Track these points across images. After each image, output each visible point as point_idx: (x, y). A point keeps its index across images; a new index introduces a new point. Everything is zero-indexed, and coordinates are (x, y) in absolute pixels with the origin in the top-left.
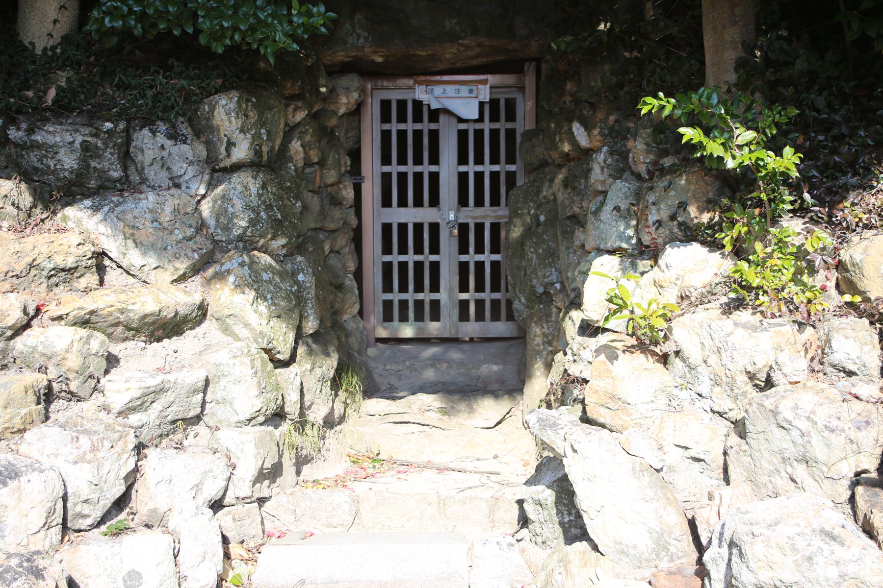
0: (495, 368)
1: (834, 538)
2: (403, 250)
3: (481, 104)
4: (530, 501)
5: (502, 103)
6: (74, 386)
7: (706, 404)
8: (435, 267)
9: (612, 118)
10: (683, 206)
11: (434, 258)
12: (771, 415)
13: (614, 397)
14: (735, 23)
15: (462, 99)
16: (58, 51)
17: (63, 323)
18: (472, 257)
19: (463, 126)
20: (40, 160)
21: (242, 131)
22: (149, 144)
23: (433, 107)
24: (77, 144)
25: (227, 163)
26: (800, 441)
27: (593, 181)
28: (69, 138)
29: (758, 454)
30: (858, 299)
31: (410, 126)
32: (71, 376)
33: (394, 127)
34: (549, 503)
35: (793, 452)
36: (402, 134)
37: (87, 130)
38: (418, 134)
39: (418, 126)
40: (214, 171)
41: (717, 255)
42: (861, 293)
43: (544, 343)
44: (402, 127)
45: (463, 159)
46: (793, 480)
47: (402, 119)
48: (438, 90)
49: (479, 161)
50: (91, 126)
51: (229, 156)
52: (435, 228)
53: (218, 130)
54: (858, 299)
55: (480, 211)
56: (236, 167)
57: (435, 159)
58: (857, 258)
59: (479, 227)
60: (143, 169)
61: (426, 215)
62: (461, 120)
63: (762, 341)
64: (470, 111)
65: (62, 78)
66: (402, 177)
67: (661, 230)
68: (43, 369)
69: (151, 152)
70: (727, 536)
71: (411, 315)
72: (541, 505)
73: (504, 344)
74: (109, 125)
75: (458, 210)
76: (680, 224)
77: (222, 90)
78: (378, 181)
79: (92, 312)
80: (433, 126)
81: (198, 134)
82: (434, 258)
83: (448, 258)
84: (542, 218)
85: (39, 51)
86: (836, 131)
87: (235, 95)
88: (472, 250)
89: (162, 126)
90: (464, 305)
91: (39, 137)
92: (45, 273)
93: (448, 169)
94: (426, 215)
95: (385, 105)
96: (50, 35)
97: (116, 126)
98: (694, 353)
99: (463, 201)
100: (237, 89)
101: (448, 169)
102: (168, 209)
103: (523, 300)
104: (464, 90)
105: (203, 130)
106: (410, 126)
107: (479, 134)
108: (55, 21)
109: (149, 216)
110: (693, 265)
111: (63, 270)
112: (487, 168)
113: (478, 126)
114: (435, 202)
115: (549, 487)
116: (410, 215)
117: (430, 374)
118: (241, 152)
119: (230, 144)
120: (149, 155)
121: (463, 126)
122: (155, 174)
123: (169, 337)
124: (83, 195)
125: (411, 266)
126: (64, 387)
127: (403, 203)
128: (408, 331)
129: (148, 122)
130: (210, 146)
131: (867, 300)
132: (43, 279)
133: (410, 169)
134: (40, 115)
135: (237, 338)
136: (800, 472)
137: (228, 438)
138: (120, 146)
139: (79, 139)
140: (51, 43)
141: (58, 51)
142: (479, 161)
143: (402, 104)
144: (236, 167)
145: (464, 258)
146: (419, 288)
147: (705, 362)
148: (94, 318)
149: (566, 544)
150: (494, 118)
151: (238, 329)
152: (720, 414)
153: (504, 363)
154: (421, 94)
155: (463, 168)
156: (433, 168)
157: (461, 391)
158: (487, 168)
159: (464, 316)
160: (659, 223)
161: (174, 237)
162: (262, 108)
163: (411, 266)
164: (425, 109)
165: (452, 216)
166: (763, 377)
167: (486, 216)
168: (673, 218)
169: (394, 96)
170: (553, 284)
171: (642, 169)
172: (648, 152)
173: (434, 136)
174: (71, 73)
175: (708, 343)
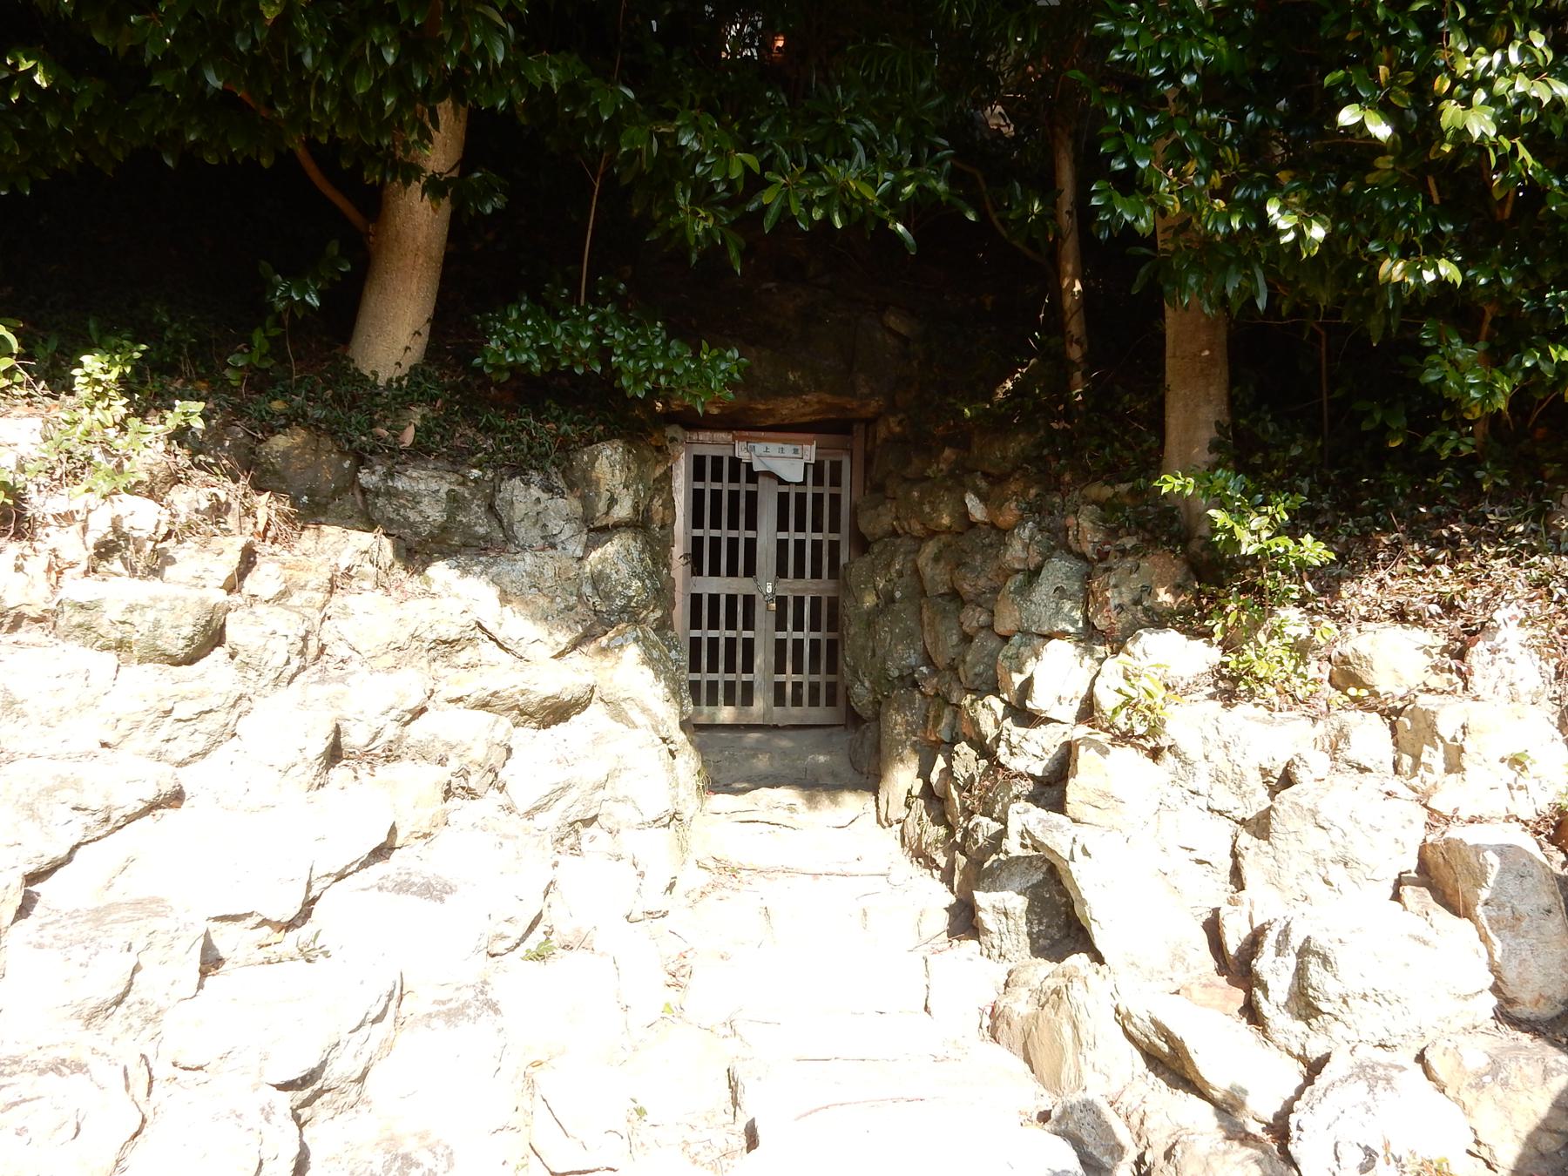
0: (822, 759)
1: (1425, 943)
2: (714, 624)
3: (806, 465)
4: (990, 909)
5: (827, 466)
6: (473, 782)
7: (1202, 802)
8: (749, 645)
9: (1033, 492)
10: (1148, 590)
11: (748, 634)
12: (1309, 814)
13: (1105, 795)
14: (1210, 402)
15: (786, 460)
16: (404, 383)
17: (461, 704)
18: (790, 635)
19: (784, 489)
20: (397, 511)
21: (626, 487)
22: (522, 496)
23: (756, 469)
24: (442, 494)
25: (610, 521)
26: (1339, 841)
27: (1008, 557)
28: (434, 486)
29: (1285, 856)
30: (1364, 693)
31: (725, 486)
32: (473, 769)
33: (708, 486)
34: (1018, 912)
35: (1329, 853)
36: (716, 494)
37: (453, 477)
38: (734, 496)
39: (734, 487)
40: (590, 530)
41: (1200, 643)
42: (1365, 686)
43: (906, 733)
44: (717, 486)
45: (782, 525)
46: (1327, 882)
47: (717, 477)
48: (760, 448)
49: (800, 527)
50: (456, 472)
51: (607, 513)
52: (749, 600)
53: (598, 484)
54: (1364, 693)
55: (799, 584)
56: (617, 527)
57: (752, 524)
58: (1363, 651)
59: (799, 602)
60: (511, 525)
61: (739, 586)
62: (781, 482)
63: (1261, 735)
64: (792, 471)
65: (416, 415)
66: (715, 542)
67: (1123, 615)
68: (442, 761)
69: (522, 506)
70: (1296, 941)
71: (721, 698)
72: (1006, 914)
73: (822, 732)
74: (476, 473)
75: (776, 582)
76: (1146, 610)
77: (607, 437)
78: (773, 549)
79: (494, 694)
80: (751, 487)
81: (572, 486)
82: (748, 634)
83: (763, 636)
84: (898, 594)
85: (381, 382)
86: (1321, 521)
87: (618, 443)
88: (790, 626)
89: (536, 477)
90: (779, 688)
91: (401, 484)
92: (426, 645)
93: (767, 535)
94: (739, 586)
95: (699, 462)
96: (398, 364)
97: (485, 474)
98: (1193, 750)
99: (781, 572)
100: (620, 437)
101: (767, 535)
102: (549, 572)
103: (867, 684)
104: (789, 449)
105: (579, 483)
106: (725, 486)
107: (801, 498)
108: (407, 348)
109: (526, 580)
110: (1172, 655)
111: (444, 642)
112: (809, 536)
113: (801, 490)
114: (750, 571)
115: (1019, 893)
116: (721, 586)
117: (762, 763)
118: (623, 511)
119: (613, 501)
120: (520, 509)
121: (784, 489)
122: (524, 532)
123: (556, 723)
124: (441, 553)
125: (722, 642)
126: (463, 783)
127: (715, 571)
128: (726, 714)
129: (518, 470)
130: (587, 503)
131: (1376, 694)
132: (424, 653)
133: (724, 533)
134: (399, 458)
135: (633, 725)
136: (1337, 873)
137: (631, 842)
138: (486, 496)
139: (445, 487)
140: (399, 373)
141: (404, 383)
142: (800, 527)
143: (717, 461)
144: (617, 527)
145: (781, 635)
146: (730, 668)
147: (1206, 757)
148: (494, 701)
149: (1037, 951)
150: (818, 481)
151: (635, 714)
152: (1220, 813)
153: (829, 753)
154: (742, 453)
155: (782, 535)
156: (750, 534)
157: (814, 784)
158: (809, 536)
159: (779, 699)
160: (1120, 607)
161: (555, 606)
162: (641, 461)
163: (722, 642)
164: (743, 468)
165: (769, 589)
166: (1278, 773)
167: (805, 590)
168: (1137, 602)
169: (709, 451)
170: (913, 669)
171: (1088, 549)
172: (1097, 531)
173: (752, 498)
174: (427, 410)
175: (1212, 734)
